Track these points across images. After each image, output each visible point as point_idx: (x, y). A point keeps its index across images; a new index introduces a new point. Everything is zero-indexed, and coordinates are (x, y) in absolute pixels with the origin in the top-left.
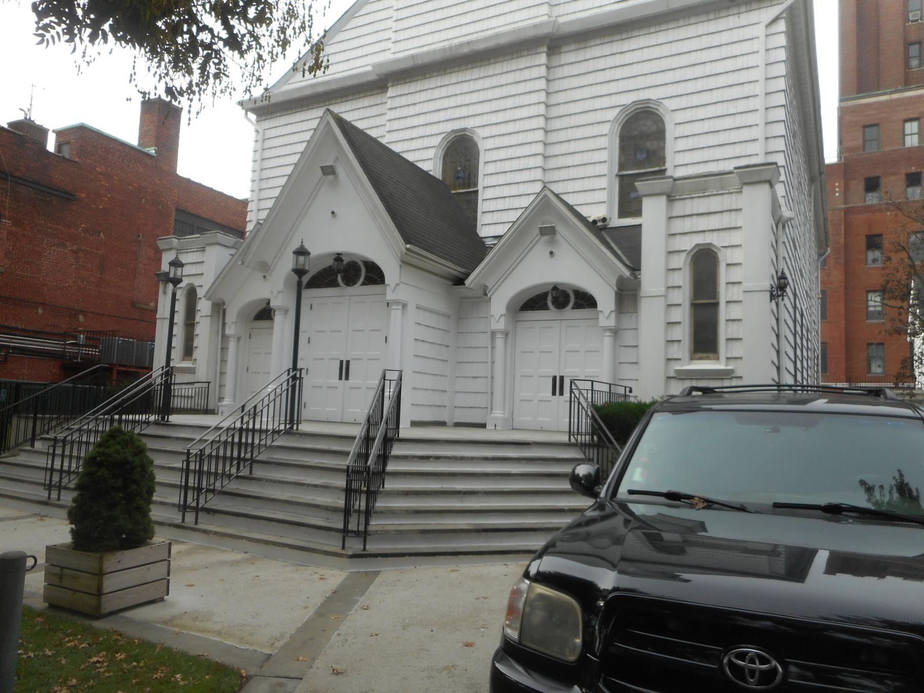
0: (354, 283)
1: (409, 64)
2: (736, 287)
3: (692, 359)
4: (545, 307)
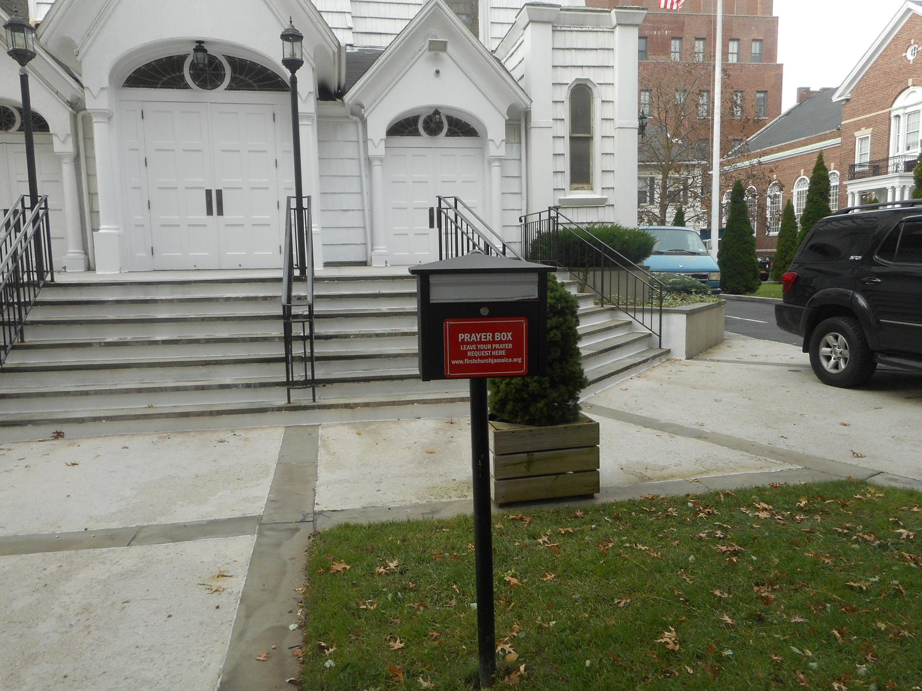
0: (214, 86)
2: (609, 123)
4: (416, 133)
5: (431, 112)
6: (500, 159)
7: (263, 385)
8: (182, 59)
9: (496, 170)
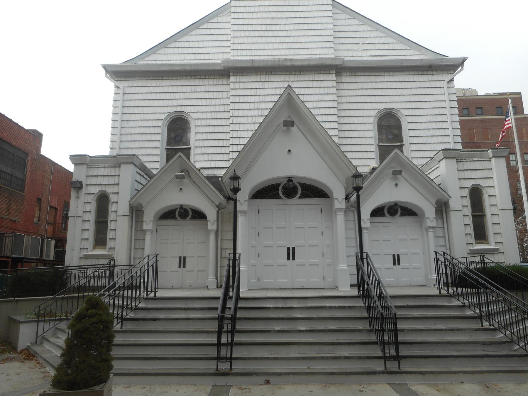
0: (293, 197)
3: (94, 249)
4: (383, 215)
6: (433, 228)
7: (368, 358)
8: (278, 185)
9: (431, 234)
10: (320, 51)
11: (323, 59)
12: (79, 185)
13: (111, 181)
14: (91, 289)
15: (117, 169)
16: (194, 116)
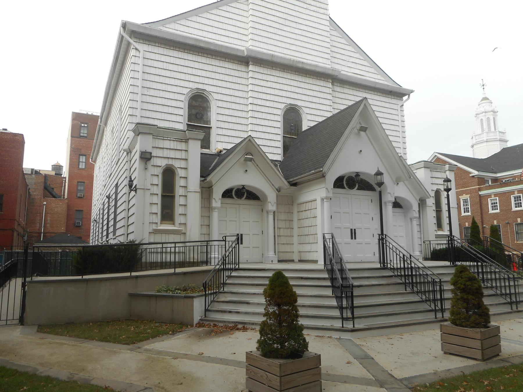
1: (269, 58)
5: (241, 187)
10: (321, 60)
11: (174, 34)
12: (148, 156)
13: (178, 155)
14: (164, 264)
15: (183, 144)
16: (216, 96)
